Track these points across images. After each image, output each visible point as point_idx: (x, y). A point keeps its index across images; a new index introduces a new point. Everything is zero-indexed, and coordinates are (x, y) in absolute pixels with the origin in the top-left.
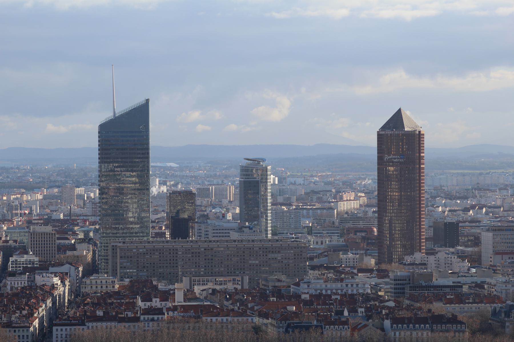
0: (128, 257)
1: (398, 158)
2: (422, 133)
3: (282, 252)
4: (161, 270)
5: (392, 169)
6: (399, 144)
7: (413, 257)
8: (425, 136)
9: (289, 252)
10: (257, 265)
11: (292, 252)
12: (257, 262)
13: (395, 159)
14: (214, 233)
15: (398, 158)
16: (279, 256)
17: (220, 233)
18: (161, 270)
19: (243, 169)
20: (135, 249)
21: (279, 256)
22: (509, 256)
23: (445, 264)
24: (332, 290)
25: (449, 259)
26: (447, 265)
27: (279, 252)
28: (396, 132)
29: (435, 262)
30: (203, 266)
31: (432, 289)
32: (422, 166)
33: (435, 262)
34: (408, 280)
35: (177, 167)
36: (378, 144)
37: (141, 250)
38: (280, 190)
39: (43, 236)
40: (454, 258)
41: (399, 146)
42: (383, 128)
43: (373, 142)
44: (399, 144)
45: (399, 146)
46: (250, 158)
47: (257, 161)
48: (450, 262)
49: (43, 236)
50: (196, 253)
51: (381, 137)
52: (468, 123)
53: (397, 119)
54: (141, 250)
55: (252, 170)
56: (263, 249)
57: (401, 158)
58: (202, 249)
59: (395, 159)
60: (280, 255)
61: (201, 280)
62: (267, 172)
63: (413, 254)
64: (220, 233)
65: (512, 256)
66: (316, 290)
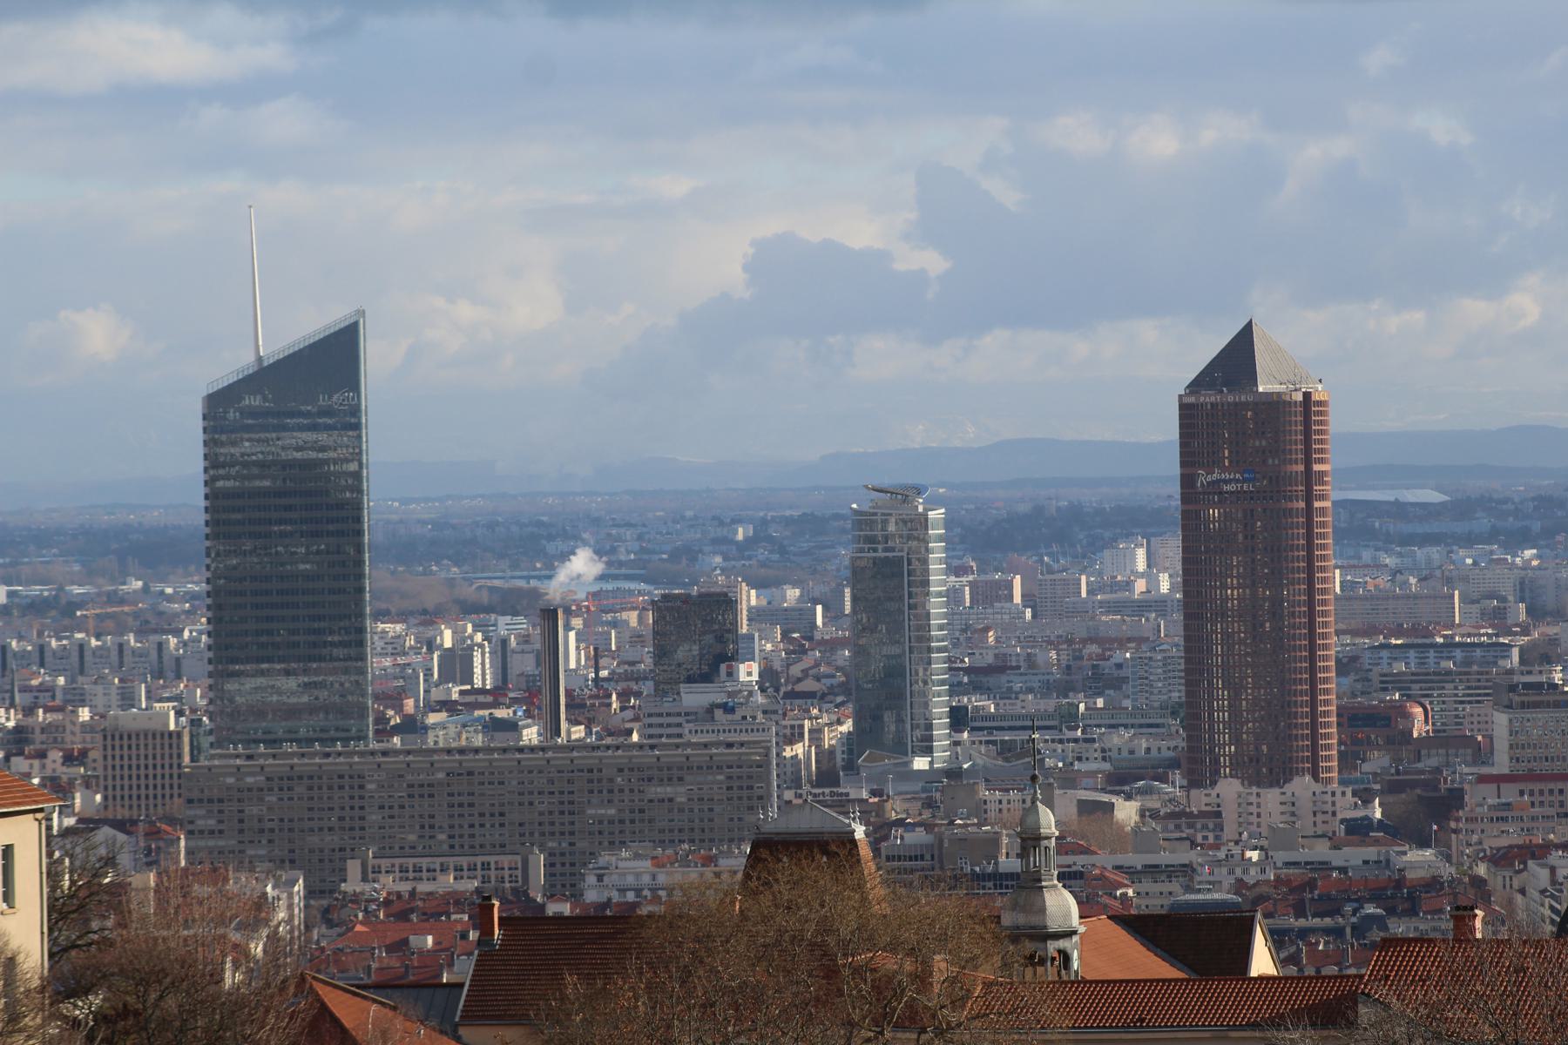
0: (210, 801)
1: (1237, 481)
2: (1316, 397)
3: (688, 778)
4: (314, 840)
5: (1214, 513)
6: (1243, 435)
7: (1214, 793)
8: (1331, 409)
9: (710, 778)
10: (611, 822)
11: (720, 777)
12: (612, 811)
13: (1226, 482)
14: (650, 726)
15: (1237, 481)
16: (680, 794)
17: (669, 725)
18: (314, 840)
19: (860, 522)
20: (231, 775)
21: (680, 794)
22: (1521, 786)
23: (1315, 814)
24: (638, 891)
25: (1328, 798)
26: (1320, 817)
27: (680, 779)
28: (1230, 399)
29: (1283, 809)
30: (445, 826)
31: (991, 884)
32: (1317, 504)
33: (1283, 809)
34: (928, 857)
35: (1442, 504)
36: (1182, 435)
37: (250, 780)
38: (1522, 583)
39: (142, 742)
40: (1343, 793)
41: (1243, 442)
42: (1196, 385)
43: (1170, 431)
44: (1243, 435)
45: (1243, 442)
46: (877, 483)
47: (904, 495)
48: (1329, 808)
49: (142, 742)
50: (422, 786)
51: (1189, 413)
52: (1457, 360)
53: (1238, 357)
54: (250, 780)
55: (885, 522)
56: (631, 770)
57: (1245, 480)
58: (441, 775)
59: (1226, 482)
60: (682, 789)
61: (493, 866)
62: (926, 528)
63: (1214, 783)
64: (669, 725)
65: (1560, 785)
66: (622, 891)
